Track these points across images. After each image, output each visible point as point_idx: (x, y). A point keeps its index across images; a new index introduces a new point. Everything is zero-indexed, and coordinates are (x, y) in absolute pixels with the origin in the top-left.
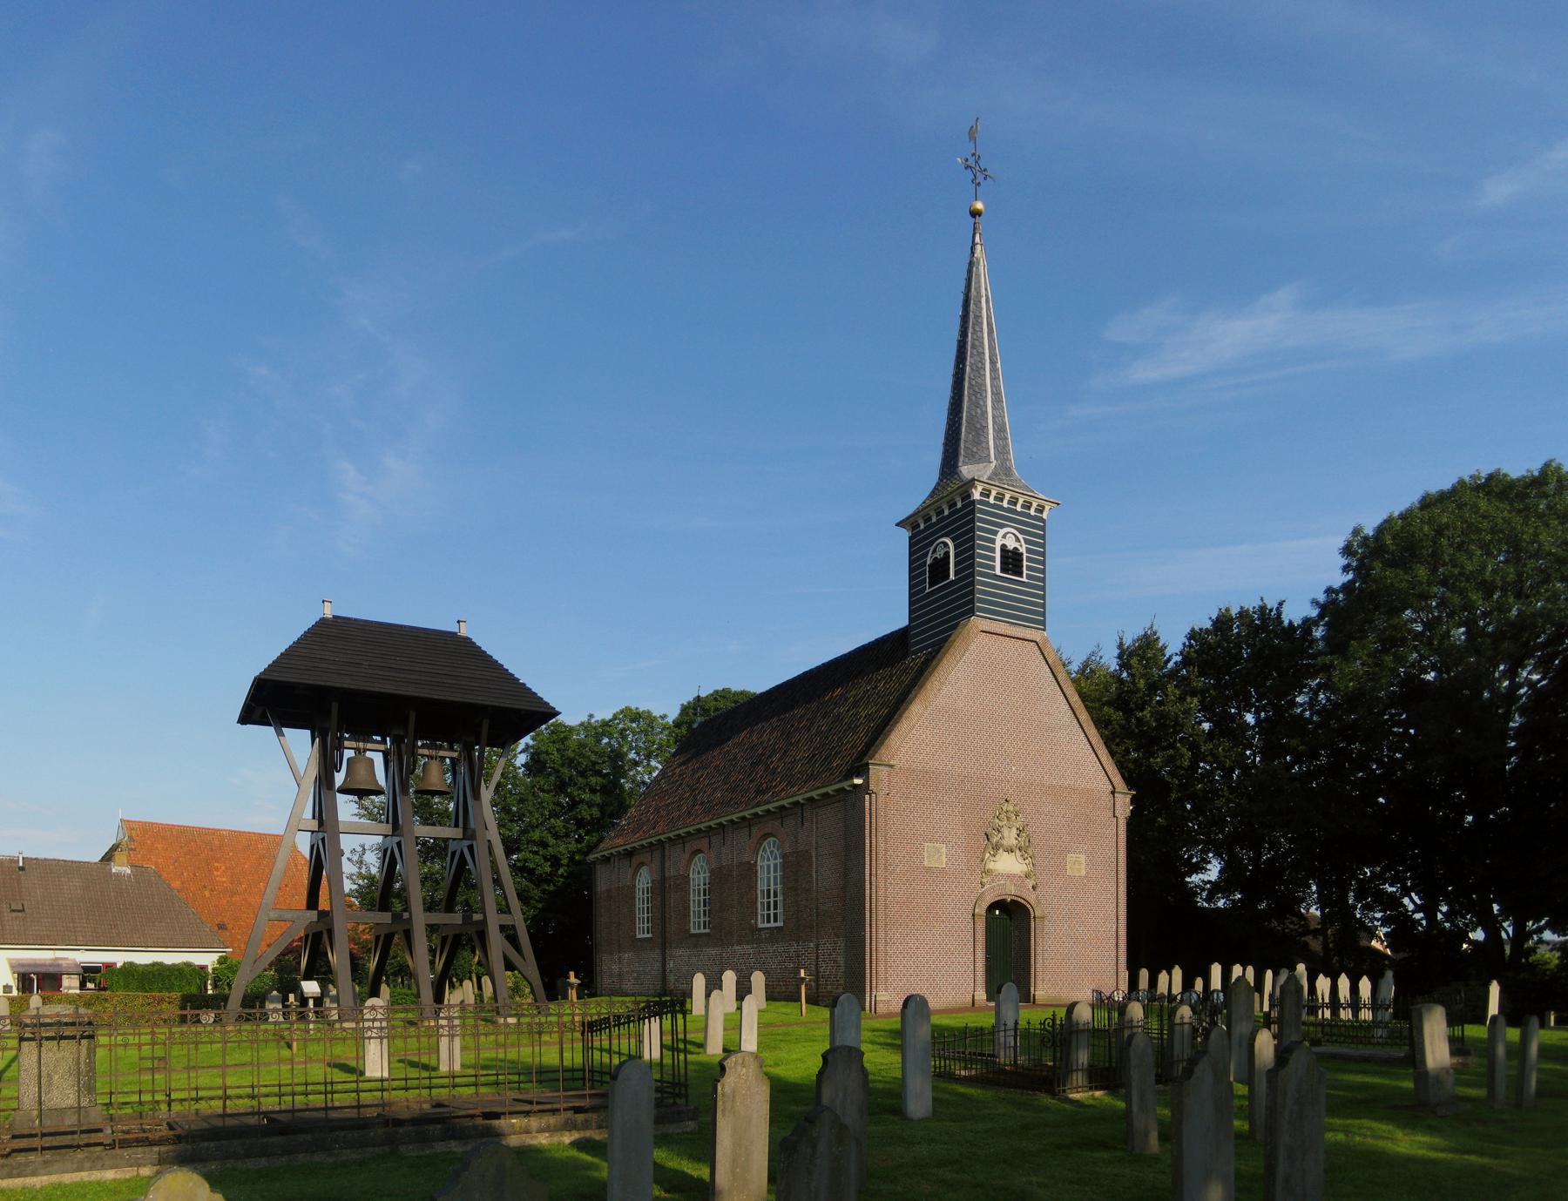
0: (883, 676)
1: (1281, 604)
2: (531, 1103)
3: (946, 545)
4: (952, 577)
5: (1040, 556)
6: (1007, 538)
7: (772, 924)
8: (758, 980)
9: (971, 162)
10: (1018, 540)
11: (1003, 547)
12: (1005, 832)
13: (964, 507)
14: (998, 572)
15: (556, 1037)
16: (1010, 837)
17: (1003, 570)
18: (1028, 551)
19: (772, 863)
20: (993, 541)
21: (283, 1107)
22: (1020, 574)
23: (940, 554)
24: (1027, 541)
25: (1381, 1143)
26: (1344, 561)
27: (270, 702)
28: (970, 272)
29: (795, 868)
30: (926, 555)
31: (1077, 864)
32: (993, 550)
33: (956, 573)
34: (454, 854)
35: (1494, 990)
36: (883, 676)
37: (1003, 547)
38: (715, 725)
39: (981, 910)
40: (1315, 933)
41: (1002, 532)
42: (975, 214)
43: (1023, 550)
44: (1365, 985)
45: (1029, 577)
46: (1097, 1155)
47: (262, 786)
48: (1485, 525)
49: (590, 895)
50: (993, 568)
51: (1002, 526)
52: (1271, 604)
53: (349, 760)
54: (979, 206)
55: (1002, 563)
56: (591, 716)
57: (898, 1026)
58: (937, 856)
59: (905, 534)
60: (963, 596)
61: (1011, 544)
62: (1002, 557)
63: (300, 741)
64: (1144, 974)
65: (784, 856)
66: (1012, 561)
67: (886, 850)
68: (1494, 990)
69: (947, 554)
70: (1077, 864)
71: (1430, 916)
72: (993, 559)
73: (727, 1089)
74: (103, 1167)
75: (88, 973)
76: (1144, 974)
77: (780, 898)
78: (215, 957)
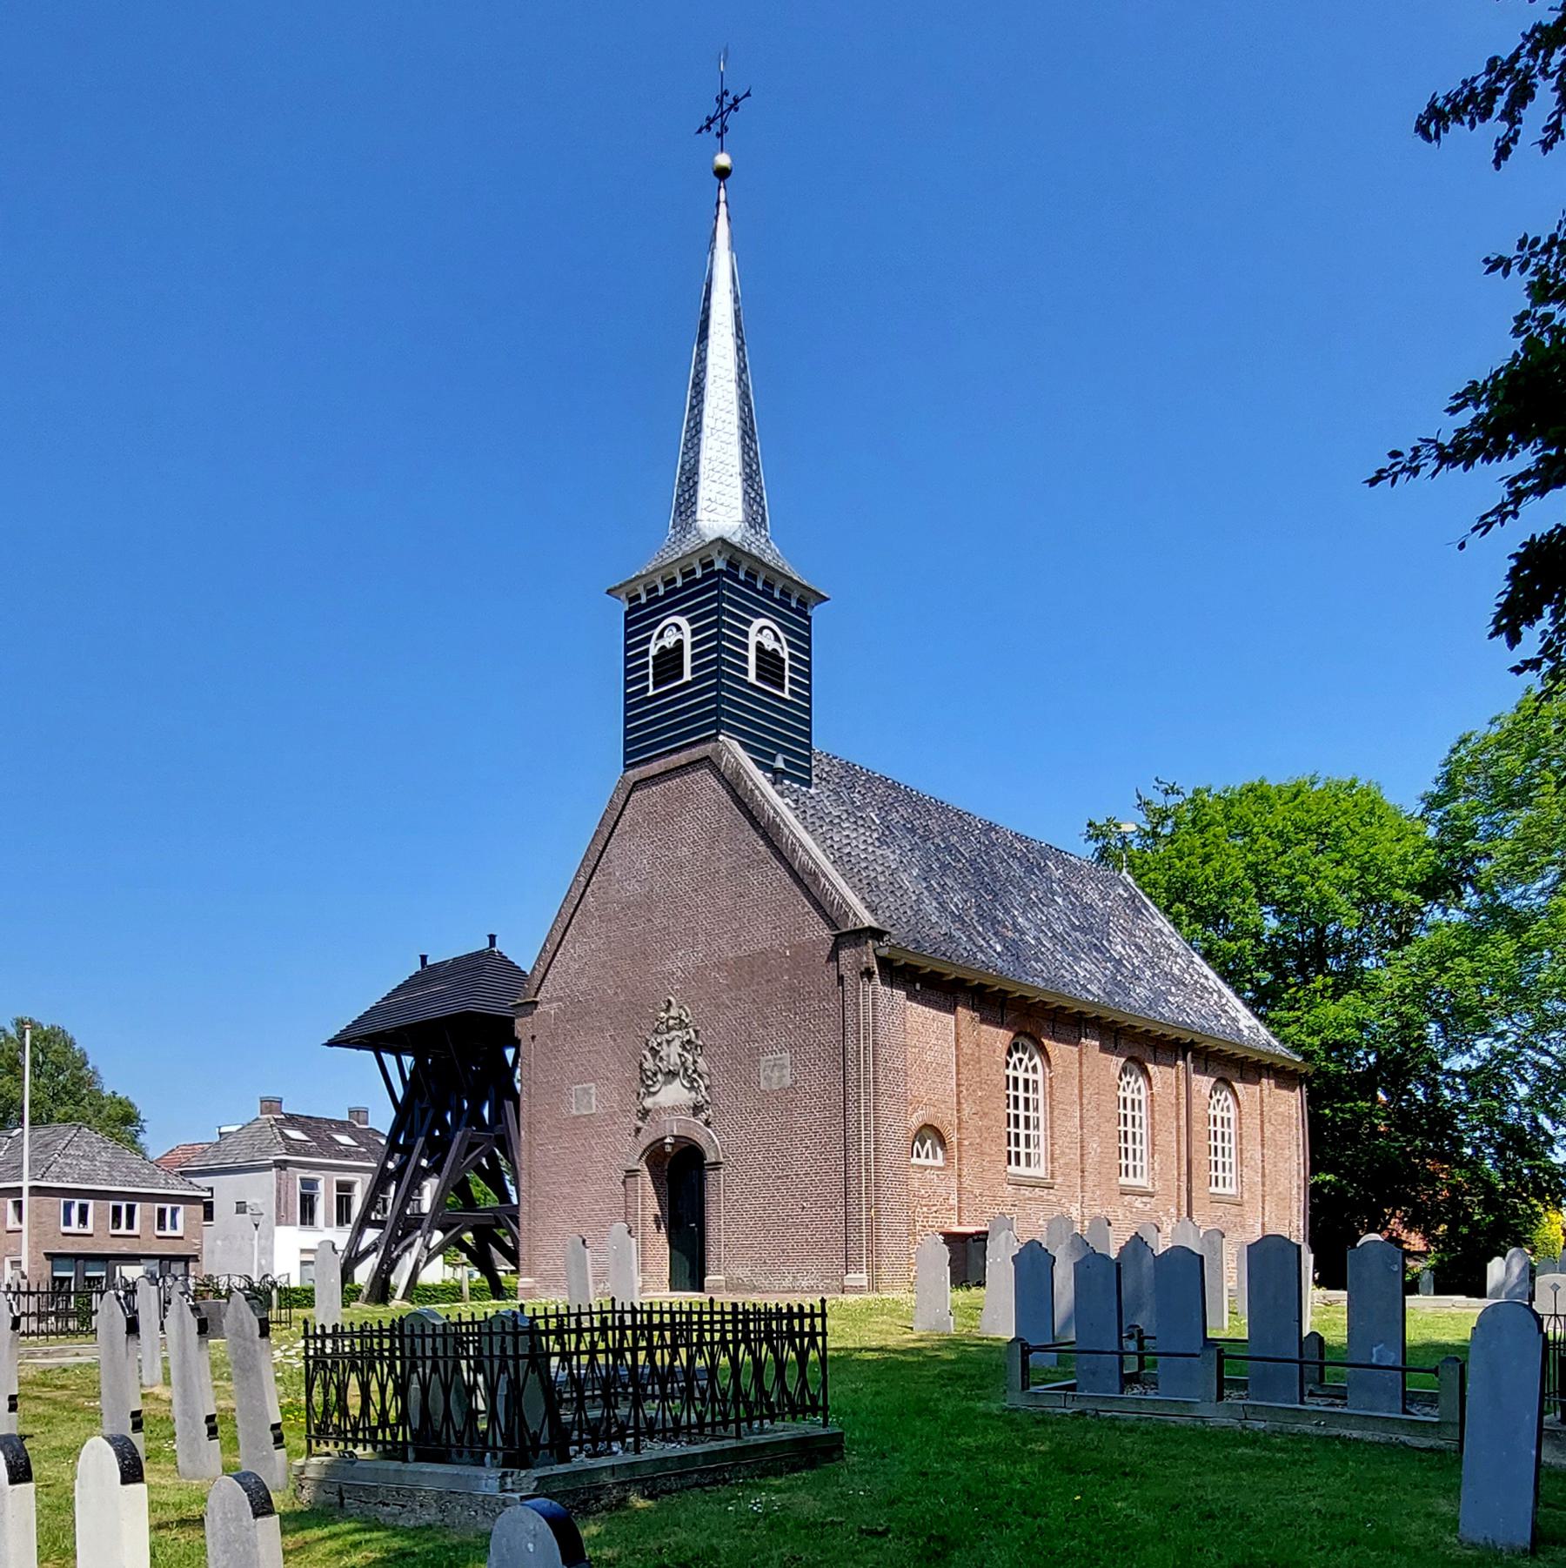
1: (1499, 264)
2: (1178, 1127)
3: (679, 628)
4: (687, 677)
5: (804, 669)
8: (1229, 1319)
9: (716, 128)
10: (777, 639)
14: (752, 677)
17: (759, 677)
20: (746, 634)
21: (298, 1507)
22: (782, 688)
23: (669, 641)
24: (790, 644)
25: (326, 1532)
28: (739, 801)
30: (648, 640)
32: (745, 647)
33: (694, 670)
35: (1547, 344)
40: (1517, 1104)
41: (759, 622)
42: (722, 173)
43: (785, 655)
45: (792, 692)
46: (757, 1502)
50: (745, 672)
52: (711, 1157)
54: (723, 160)
55: (758, 667)
60: (637, 729)
61: (770, 644)
62: (758, 658)
66: (769, 664)
69: (680, 643)
71: (1331, 973)
74: (336, 1523)
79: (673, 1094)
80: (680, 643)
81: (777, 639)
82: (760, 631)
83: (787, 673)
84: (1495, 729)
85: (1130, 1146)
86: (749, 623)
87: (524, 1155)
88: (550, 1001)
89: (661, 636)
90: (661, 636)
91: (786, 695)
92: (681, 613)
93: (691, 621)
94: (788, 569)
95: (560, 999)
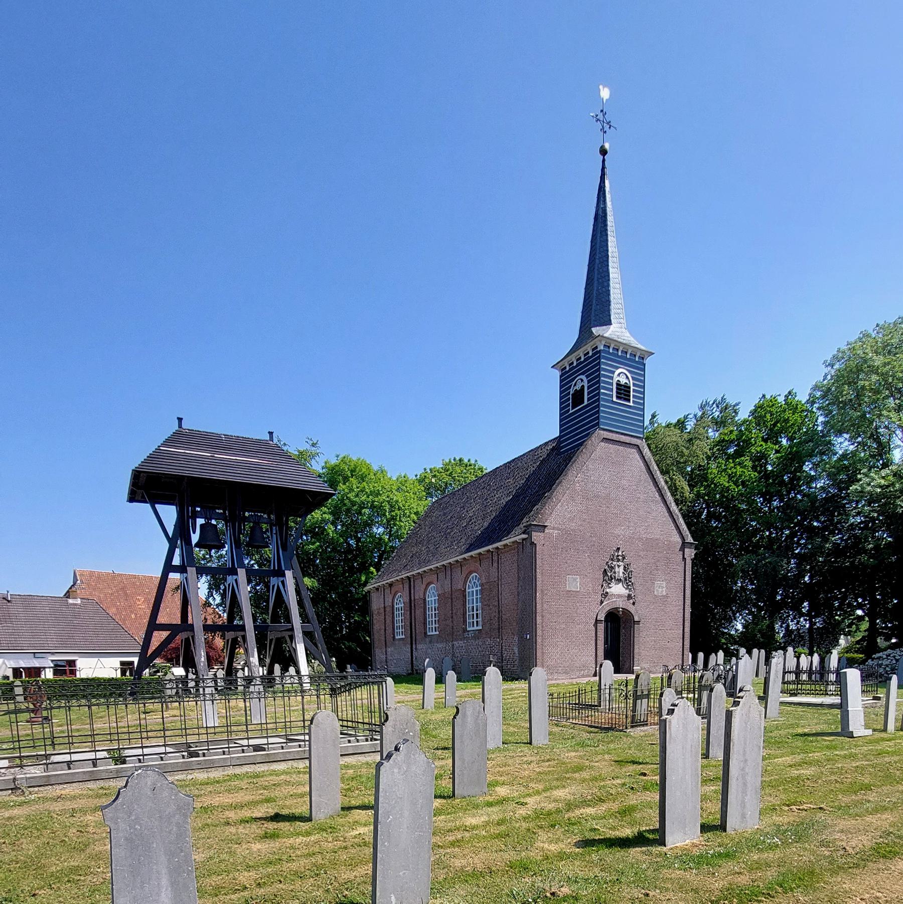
0: (545, 470)
3: (582, 380)
4: (586, 402)
6: (621, 375)
7: (475, 628)
9: (600, 116)
10: (627, 377)
11: (618, 384)
12: (617, 569)
13: (593, 355)
14: (615, 399)
15: (366, 720)
16: (620, 572)
17: (618, 397)
18: (634, 385)
19: (474, 589)
20: (612, 378)
22: (629, 400)
23: (578, 387)
26: (768, 397)
27: (148, 486)
29: (489, 592)
31: (661, 588)
32: (612, 384)
34: (273, 586)
36: (545, 470)
37: (618, 384)
38: (451, 493)
39: (602, 617)
44: (168, 686)
47: (141, 544)
48: (547, 843)
49: (531, 637)
51: (617, 368)
52: (636, 619)
53: (202, 526)
56: (764, 396)
57: (657, 826)
58: (574, 583)
59: (557, 374)
61: (623, 380)
63: (169, 513)
64: (701, 655)
65: (482, 585)
66: (623, 391)
67: (543, 653)
68: (427, 660)
69: (583, 386)
70: (661, 588)
72: (612, 390)
73: (673, 735)
75: (198, 756)
76: (701, 655)
77: (480, 612)
78: (116, 662)
79: (618, 589)
80: (583, 386)
81: (627, 377)
82: (619, 375)
83: (632, 388)
84: (150, 707)
85: (475, 620)
86: (613, 372)
87: (808, 710)
88: (554, 528)
89: (575, 385)
90: (575, 385)
91: (631, 404)
92: (582, 374)
93: (587, 377)
94: (640, 346)
95: (558, 529)
